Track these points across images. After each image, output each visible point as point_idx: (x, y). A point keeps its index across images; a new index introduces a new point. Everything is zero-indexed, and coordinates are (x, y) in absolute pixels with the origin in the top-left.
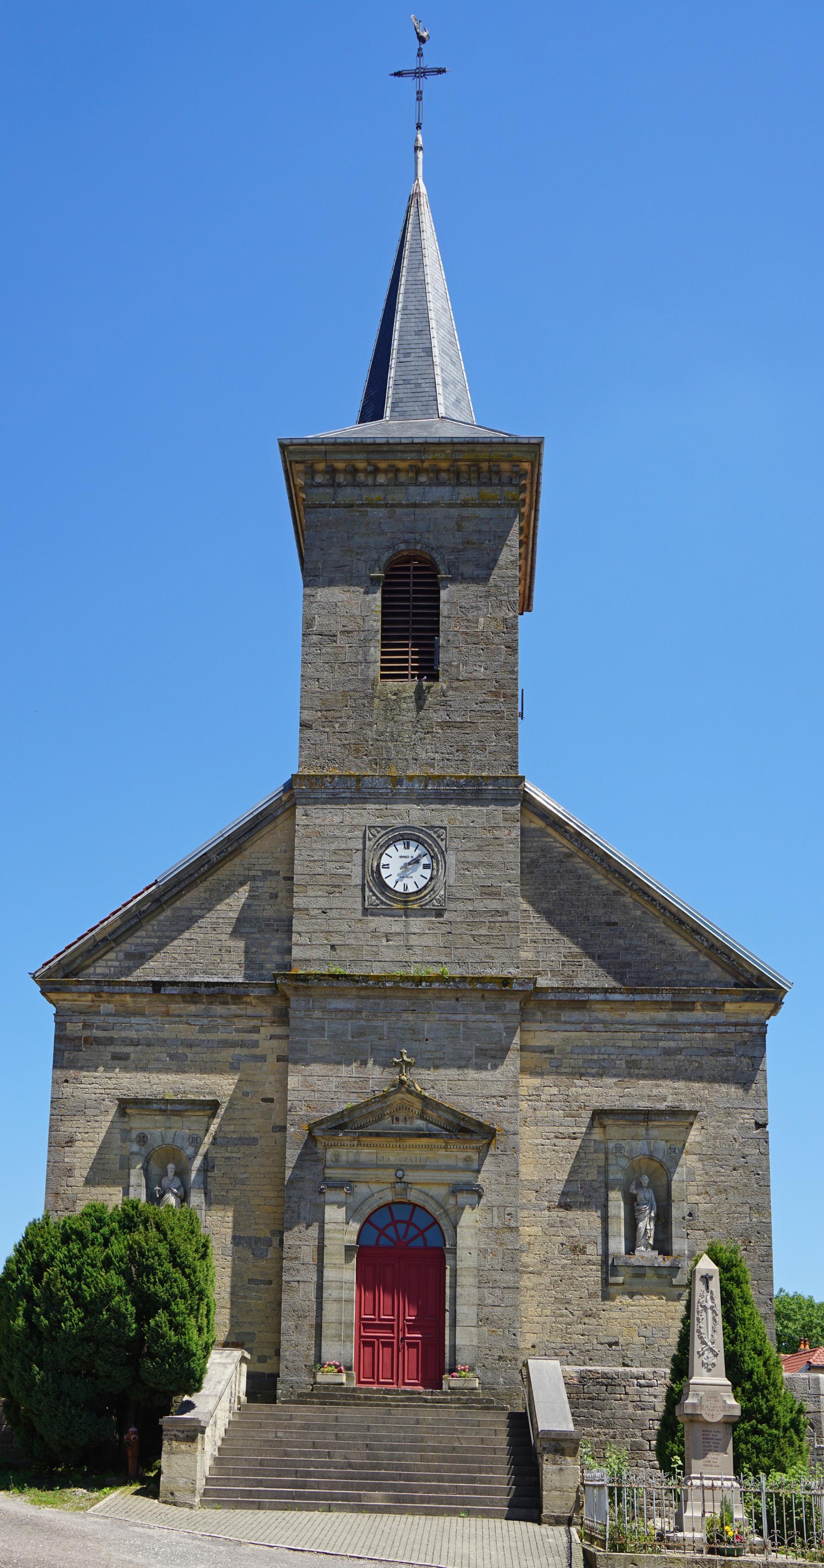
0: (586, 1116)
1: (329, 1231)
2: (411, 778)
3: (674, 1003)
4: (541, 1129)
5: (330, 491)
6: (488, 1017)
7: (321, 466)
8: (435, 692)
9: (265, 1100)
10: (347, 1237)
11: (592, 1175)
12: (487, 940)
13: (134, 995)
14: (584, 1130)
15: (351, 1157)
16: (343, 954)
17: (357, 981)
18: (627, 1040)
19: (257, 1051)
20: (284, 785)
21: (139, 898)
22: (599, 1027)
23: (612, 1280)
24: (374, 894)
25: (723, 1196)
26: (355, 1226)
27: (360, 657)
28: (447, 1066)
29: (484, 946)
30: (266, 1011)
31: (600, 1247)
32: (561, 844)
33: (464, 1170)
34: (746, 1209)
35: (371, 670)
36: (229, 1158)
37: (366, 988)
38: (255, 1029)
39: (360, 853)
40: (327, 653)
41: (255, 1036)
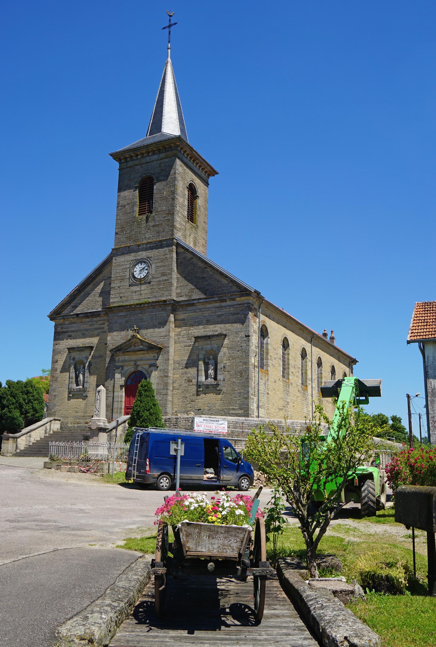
0: (193, 339)
2: (143, 244)
5: (125, 164)
6: (162, 312)
7: (122, 157)
11: (195, 357)
13: (73, 318)
15: (123, 359)
18: (206, 314)
19: (104, 330)
22: (198, 311)
23: (199, 390)
25: (234, 360)
26: (124, 379)
28: (150, 328)
31: (196, 379)
32: (189, 256)
33: (152, 360)
34: (241, 364)
37: (127, 309)
38: (104, 324)
41: (104, 326)
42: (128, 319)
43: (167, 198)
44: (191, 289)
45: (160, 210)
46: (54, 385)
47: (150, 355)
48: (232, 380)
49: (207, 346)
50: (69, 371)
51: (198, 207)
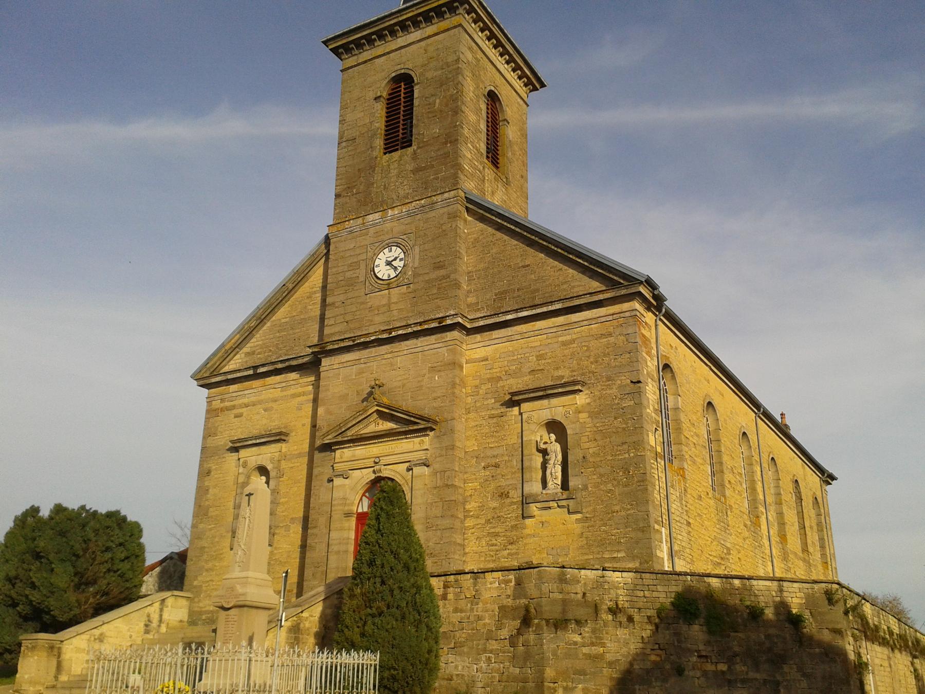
34: (625, 447)
36: (292, 468)
51: (507, 142)
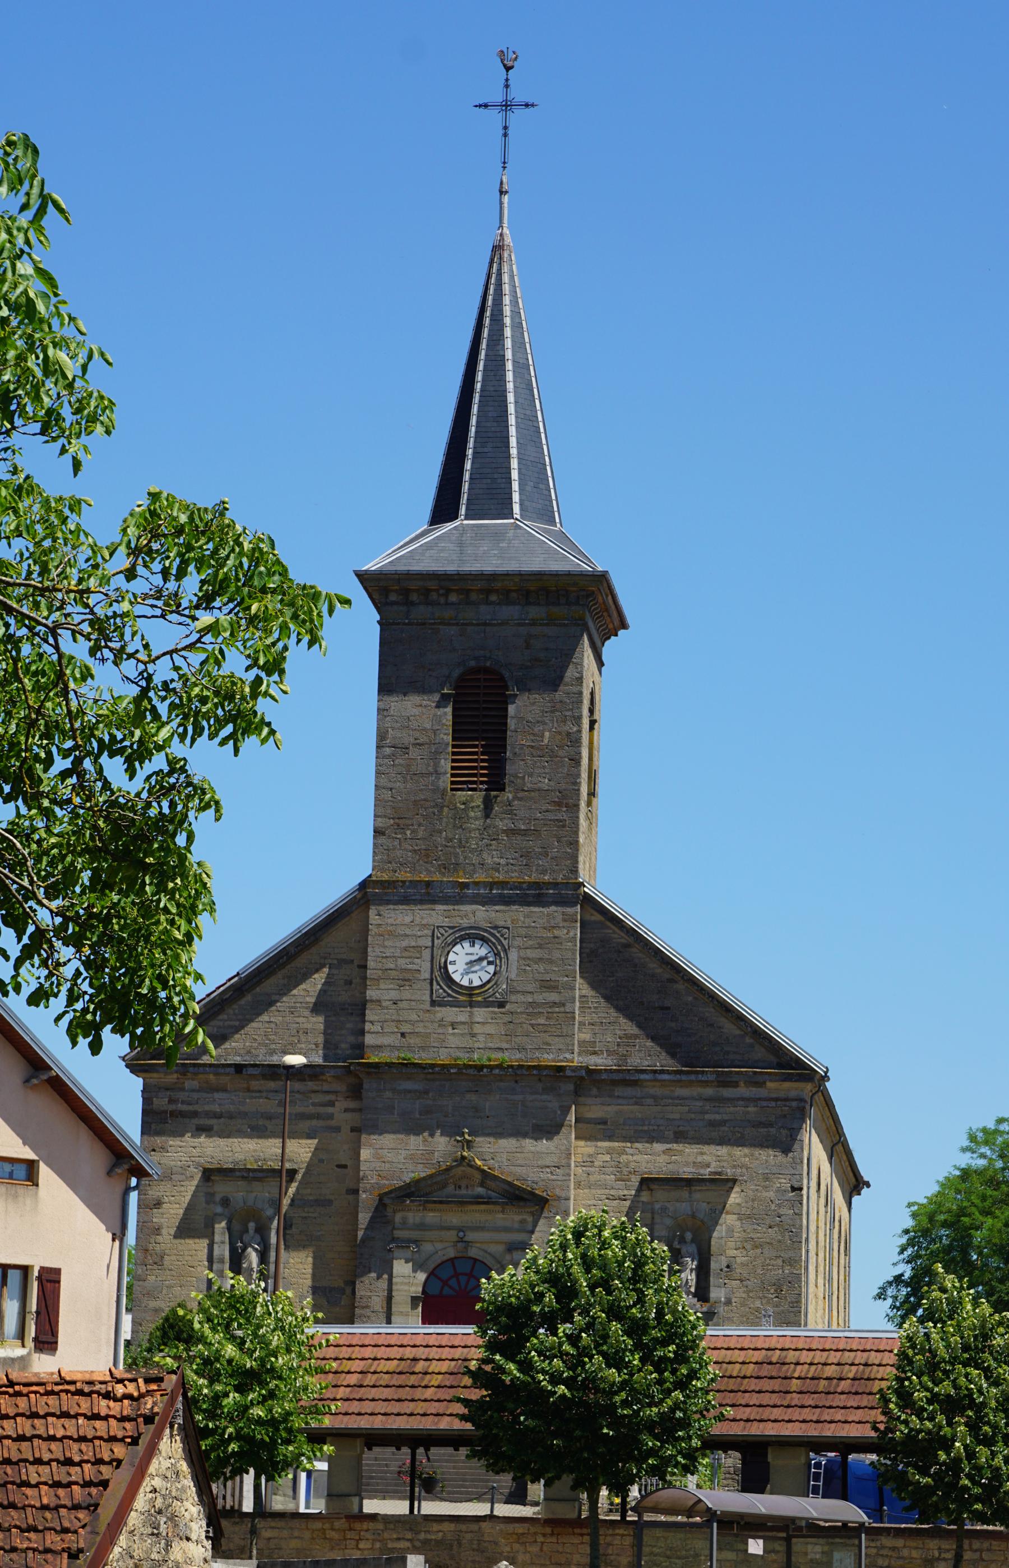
0: (635, 1181)
1: (397, 1284)
3: (718, 1082)
4: (594, 1191)
6: (544, 1097)
8: (501, 802)
9: (339, 1166)
10: (413, 1289)
12: (545, 1028)
13: (216, 1074)
14: (633, 1192)
15: (418, 1220)
16: (412, 1041)
17: (424, 1068)
19: (333, 1123)
20: (360, 884)
21: (222, 989)
22: (650, 1101)
24: (442, 988)
25: (759, 1251)
26: (422, 1276)
27: (431, 769)
29: (542, 1034)
30: (341, 1087)
33: (519, 1231)
34: (779, 1262)
35: (441, 781)
38: (331, 1104)
39: (428, 951)
40: (400, 765)
41: (330, 1110)
42: (430, 1102)
43: (553, 755)
44: (626, 1036)
45: (529, 785)
46: (152, 1279)
47: (513, 1217)
48: (753, 1303)
49: (680, 1205)
50: (207, 1233)
